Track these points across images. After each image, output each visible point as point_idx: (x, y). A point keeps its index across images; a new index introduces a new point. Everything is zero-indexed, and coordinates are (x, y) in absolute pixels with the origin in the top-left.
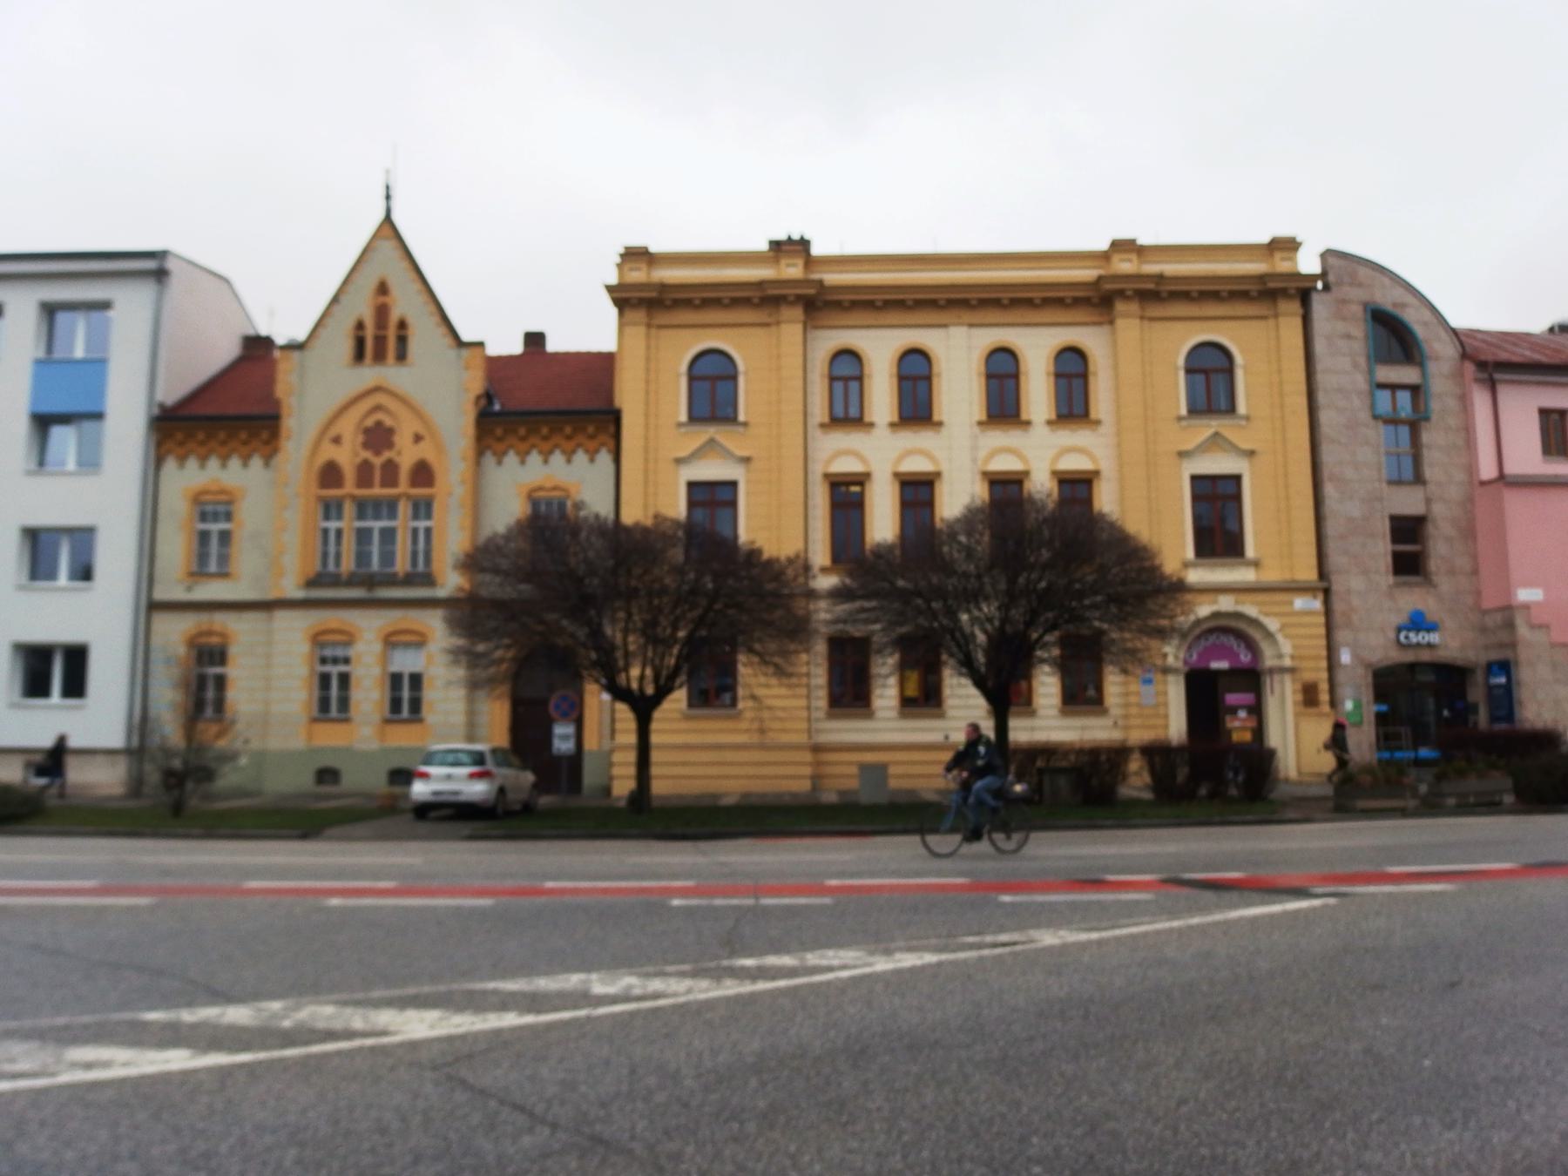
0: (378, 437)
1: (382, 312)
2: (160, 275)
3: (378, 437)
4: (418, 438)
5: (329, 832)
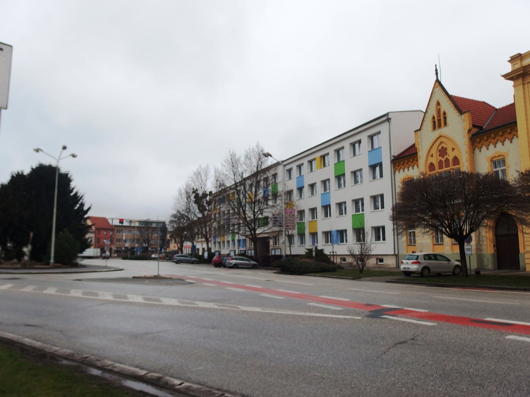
0: (443, 152)
1: (439, 111)
2: (388, 120)
3: (443, 152)
4: (453, 149)
5: (362, 279)
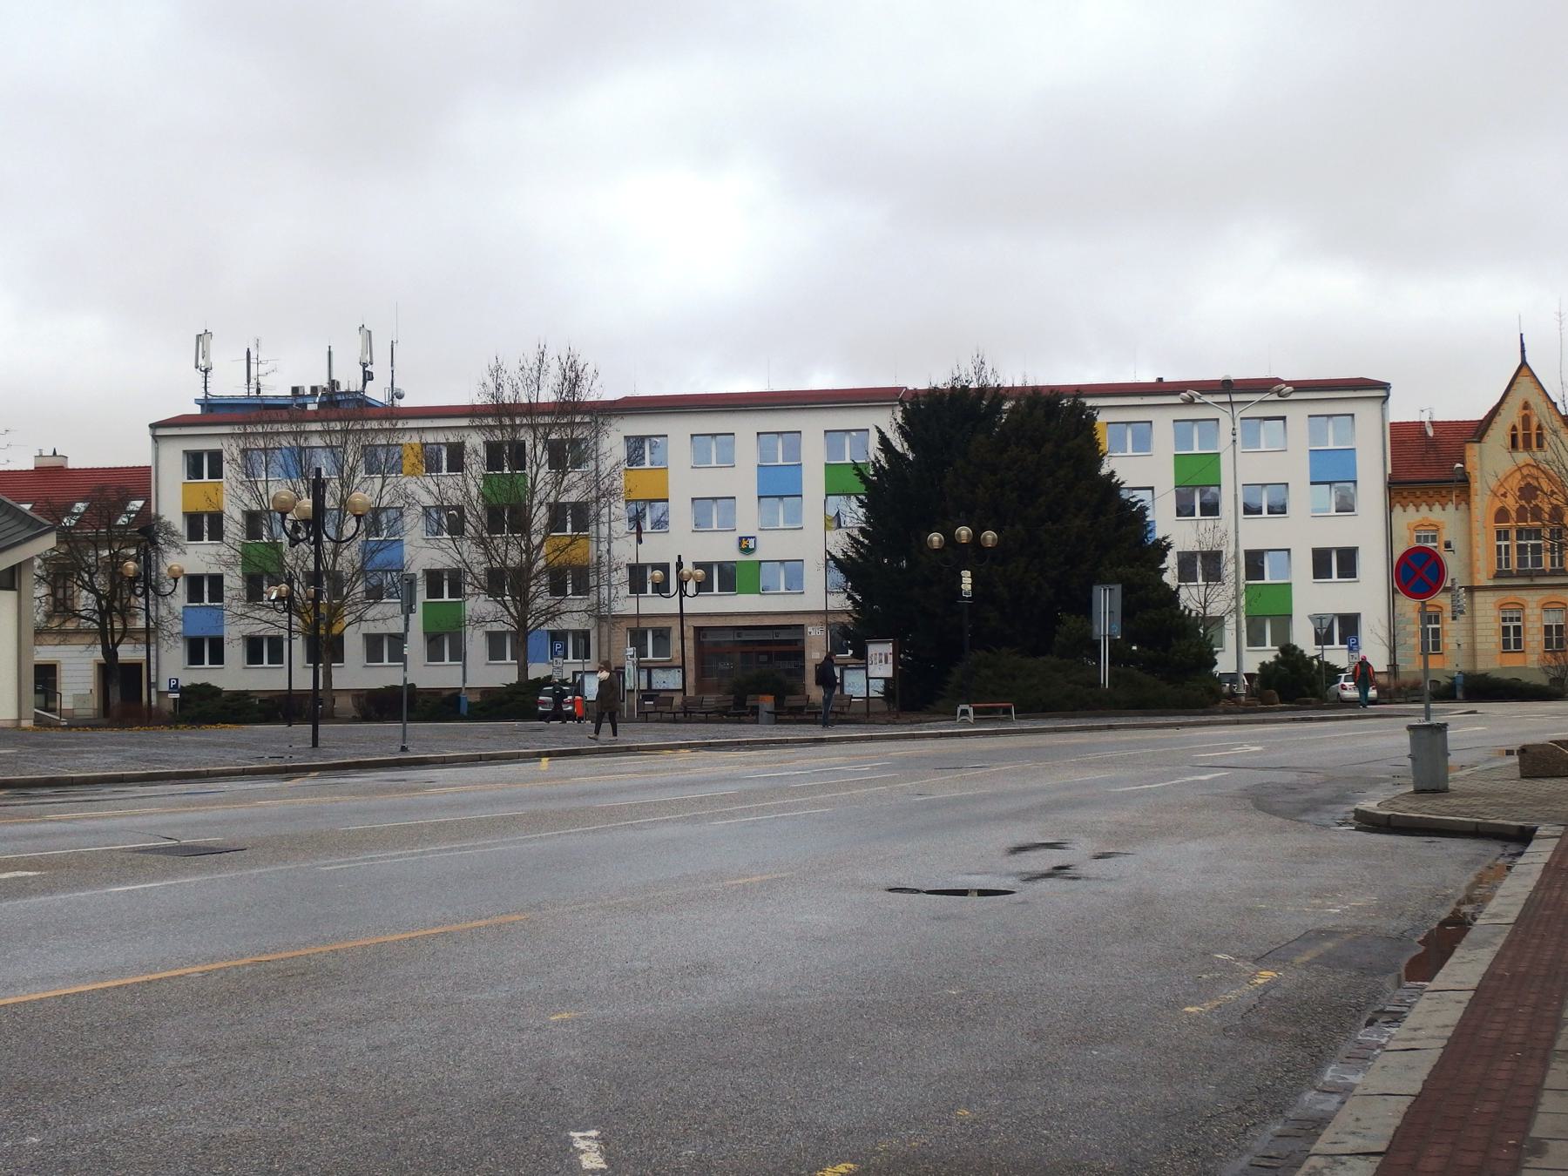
1: (1526, 420)
3: (1528, 492)
